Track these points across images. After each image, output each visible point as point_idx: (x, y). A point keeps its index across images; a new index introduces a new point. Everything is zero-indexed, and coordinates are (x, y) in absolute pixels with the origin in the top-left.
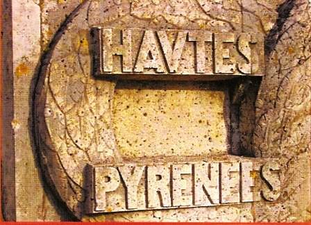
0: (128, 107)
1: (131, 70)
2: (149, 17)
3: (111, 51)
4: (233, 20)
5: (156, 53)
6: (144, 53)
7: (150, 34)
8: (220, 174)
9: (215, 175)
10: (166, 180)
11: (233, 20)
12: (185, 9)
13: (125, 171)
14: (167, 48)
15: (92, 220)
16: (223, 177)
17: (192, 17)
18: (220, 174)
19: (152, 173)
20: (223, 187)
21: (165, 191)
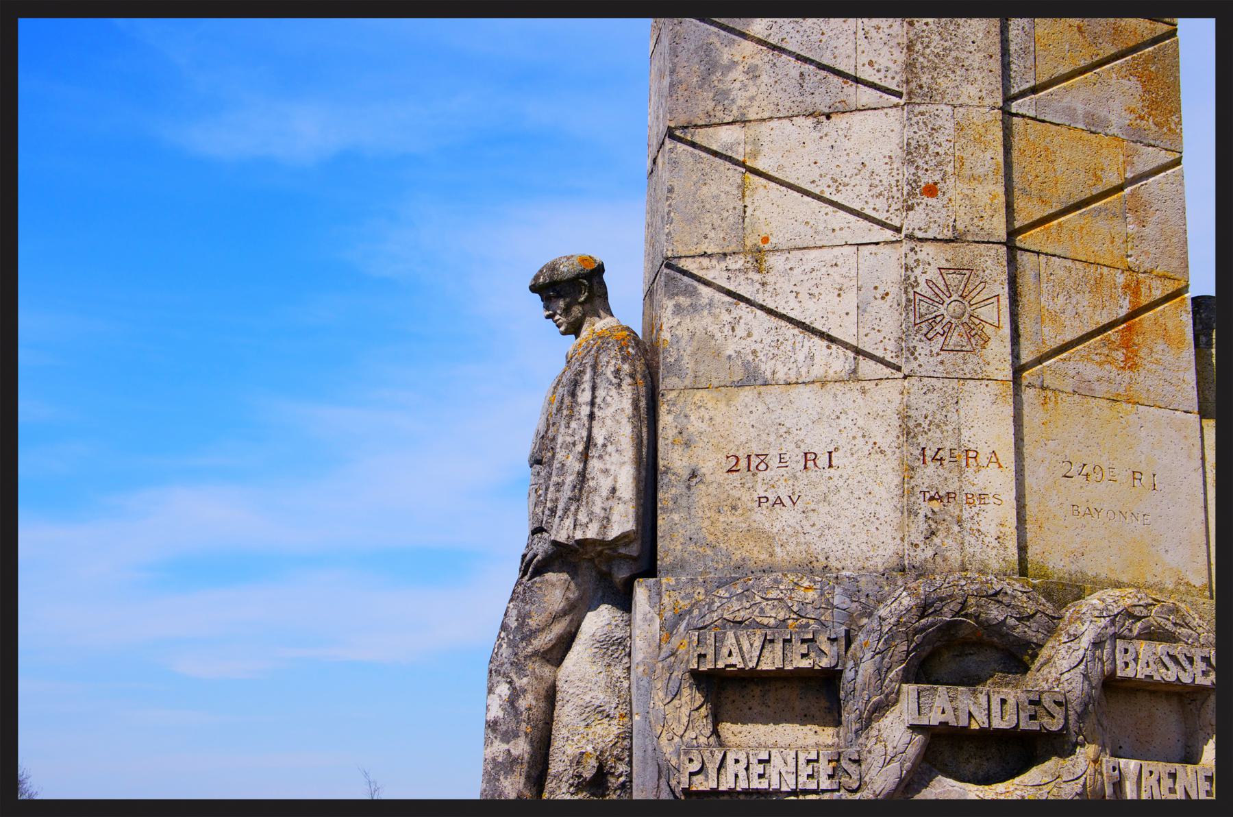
0: (734, 701)
1: (713, 667)
2: (740, 620)
3: (695, 651)
4: (823, 618)
5: (735, 650)
6: (725, 651)
7: (730, 634)
8: (797, 762)
9: (792, 762)
10: (743, 764)
11: (823, 618)
12: (775, 611)
13: (707, 754)
14: (746, 646)
15: (763, 798)
16: (799, 763)
17: (781, 617)
18: (797, 762)
19: (730, 758)
20: (799, 773)
21: (742, 774)
